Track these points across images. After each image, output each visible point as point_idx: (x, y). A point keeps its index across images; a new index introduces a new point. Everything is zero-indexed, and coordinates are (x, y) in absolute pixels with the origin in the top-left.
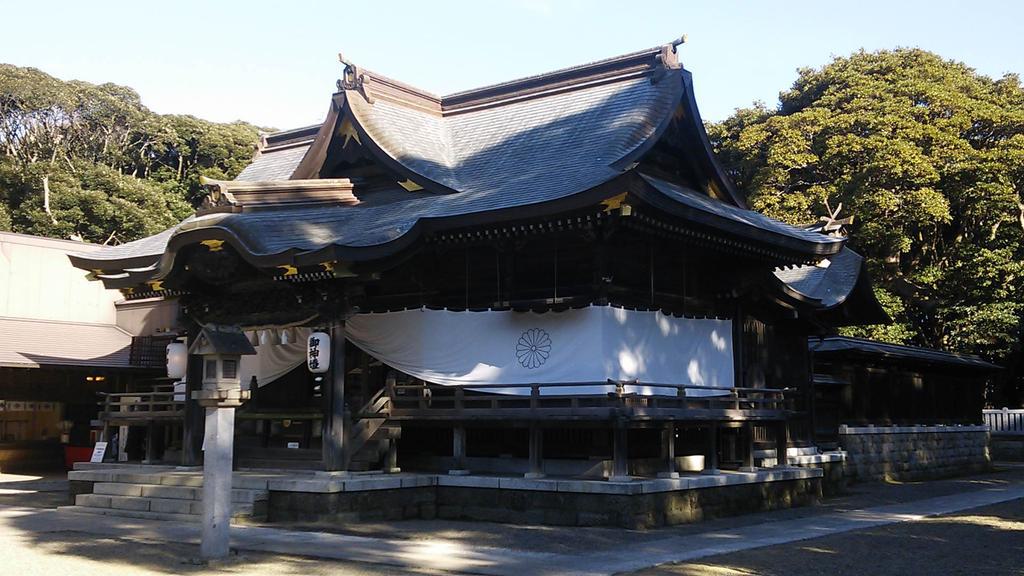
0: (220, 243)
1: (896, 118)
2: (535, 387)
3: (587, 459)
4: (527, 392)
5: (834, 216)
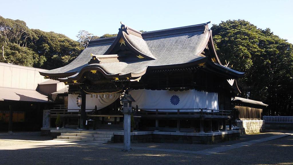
0: (96, 71)
1: (240, 40)
2: (157, 110)
3: (190, 128)
4: (176, 111)
5: (227, 65)
